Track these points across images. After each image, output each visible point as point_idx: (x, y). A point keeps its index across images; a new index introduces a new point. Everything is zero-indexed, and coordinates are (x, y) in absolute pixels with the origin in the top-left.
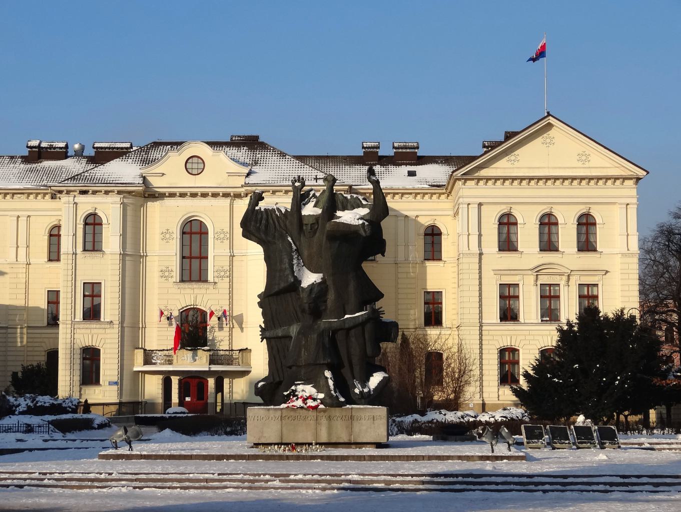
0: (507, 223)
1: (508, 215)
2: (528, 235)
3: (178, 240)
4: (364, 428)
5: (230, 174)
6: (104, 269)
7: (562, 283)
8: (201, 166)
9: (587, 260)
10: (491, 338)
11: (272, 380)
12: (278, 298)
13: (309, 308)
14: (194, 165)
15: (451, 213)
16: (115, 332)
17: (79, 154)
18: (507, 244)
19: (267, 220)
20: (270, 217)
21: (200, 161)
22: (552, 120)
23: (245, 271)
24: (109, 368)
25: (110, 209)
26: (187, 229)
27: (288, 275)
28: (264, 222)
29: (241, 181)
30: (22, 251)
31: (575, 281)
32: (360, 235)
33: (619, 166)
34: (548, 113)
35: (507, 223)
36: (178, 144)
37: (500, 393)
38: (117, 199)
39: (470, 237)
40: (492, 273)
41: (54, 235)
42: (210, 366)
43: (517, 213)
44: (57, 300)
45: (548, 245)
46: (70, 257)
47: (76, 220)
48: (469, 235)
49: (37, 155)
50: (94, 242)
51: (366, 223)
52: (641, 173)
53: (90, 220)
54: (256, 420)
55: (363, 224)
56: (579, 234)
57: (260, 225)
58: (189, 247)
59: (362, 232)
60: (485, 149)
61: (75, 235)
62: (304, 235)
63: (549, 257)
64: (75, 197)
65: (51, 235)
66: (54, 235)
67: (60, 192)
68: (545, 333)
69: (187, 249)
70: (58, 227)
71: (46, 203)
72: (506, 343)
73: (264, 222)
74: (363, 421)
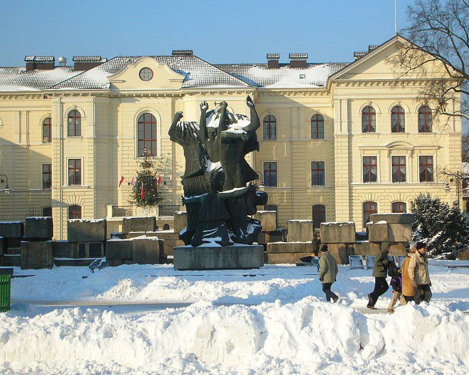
0: (368, 113)
1: (369, 108)
2: (383, 121)
5: (172, 81)
6: (82, 148)
7: (407, 156)
9: (426, 139)
10: (358, 195)
12: (194, 176)
14: (145, 75)
16: (91, 193)
17: (63, 65)
18: (368, 127)
23: (172, 159)
25: (86, 107)
29: (180, 85)
35: (368, 113)
38: (91, 99)
40: (358, 149)
41: (47, 125)
42: (160, 217)
44: (49, 171)
45: (397, 128)
46: (59, 141)
47: (62, 116)
49: (33, 66)
51: (246, 133)
55: (243, 133)
59: (243, 138)
60: (355, 58)
63: (398, 137)
64: (61, 98)
65: (44, 125)
66: (47, 125)
68: (395, 191)
70: (50, 119)
71: (41, 102)
72: (367, 198)
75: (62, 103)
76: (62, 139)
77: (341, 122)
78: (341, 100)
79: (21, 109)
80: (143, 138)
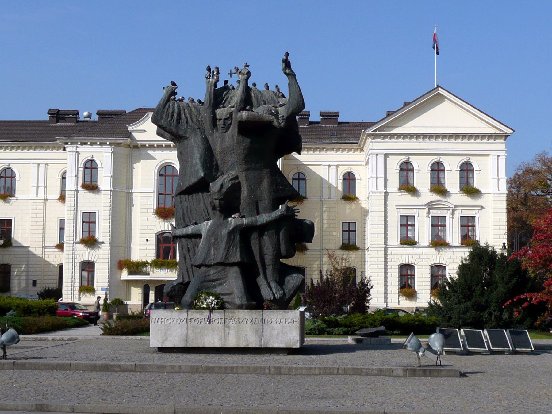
0: (406, 168)
3: (156, 181)
4: (276, 332)
6: (100, 204)
11: (181, 280)
13: (220, 204)
15: (364, 163)
18: (407, 187)
19: (179, 115)
20: (182, 113)
22: (441, 91)
24: (101, 279)
26: (163, 173)
27: (198, 170)
28: (175, 116)
30: (41, 190)
31: (459, 214)
32: (274, 127)
35: (406, 168)
37: (400, 299)
39: (378, 180)
40: (395, 207)
43: (414, 160)
45: (439, 188)
48: (377, 178)
53: (89, 165)
54: (160, 323)
56: (461, 178)
57: (171, 120)
58: (164, 186)
61: (77, 176)
62: (217, 131)
69: (162, 187)
72: (404, 260)
73: (175, 116)
74: (274, 324)
75: (78, 153)
76: (77, 191)
77: (377, 178)
78: (377, 155)
79: (40, 162)
80: (163, 192)
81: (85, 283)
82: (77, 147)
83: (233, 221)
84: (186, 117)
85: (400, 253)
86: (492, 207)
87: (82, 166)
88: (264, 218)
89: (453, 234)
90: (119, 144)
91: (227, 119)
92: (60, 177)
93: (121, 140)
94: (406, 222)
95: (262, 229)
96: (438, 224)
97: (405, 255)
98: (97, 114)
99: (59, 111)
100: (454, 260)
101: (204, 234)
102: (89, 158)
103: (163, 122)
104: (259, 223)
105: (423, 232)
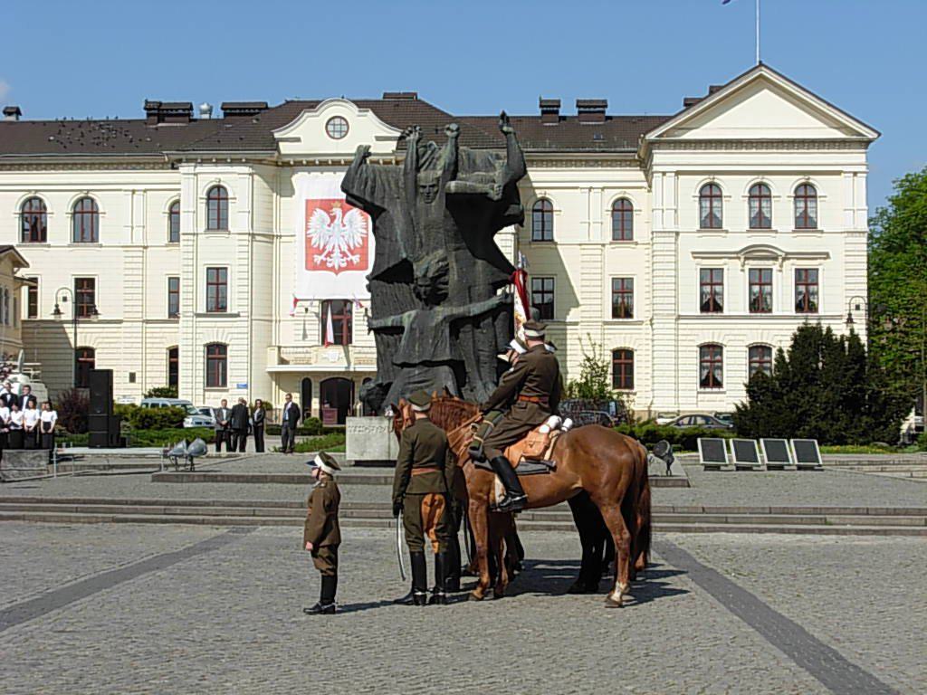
8: (345, 128)
9: (806, 242)
14: (337, 127)
21: (343, 122)
28: (369, 183)
33: (683, 126)
34: (760, 62)
36: (313, 105)
40: (691, 255)
50: (219, 219)
52: (871, 135)
63: (760, 238)
67: (180, 161)
81: (897, 511)
82: (195, 167)
83: (441, 312)
84: (383, 185)
85: (700, 326)
86: (844, 253)
87: (205, 196)
88: (476, 308)
89: (783, 294)
90: (260, 162)
91: (433, 186)
92: (167, 210)
93: (261, 155)
94: (711, 279)
95: (476, 320)
96: (760, 280)
97: (711, 330)
98: (222, 109)
99: (161, 104)
100: (780, 334)
101: (406, 325)
102: (215, 183)
103: (355, 192)
104: (471, 314)
105: (736, 294)
